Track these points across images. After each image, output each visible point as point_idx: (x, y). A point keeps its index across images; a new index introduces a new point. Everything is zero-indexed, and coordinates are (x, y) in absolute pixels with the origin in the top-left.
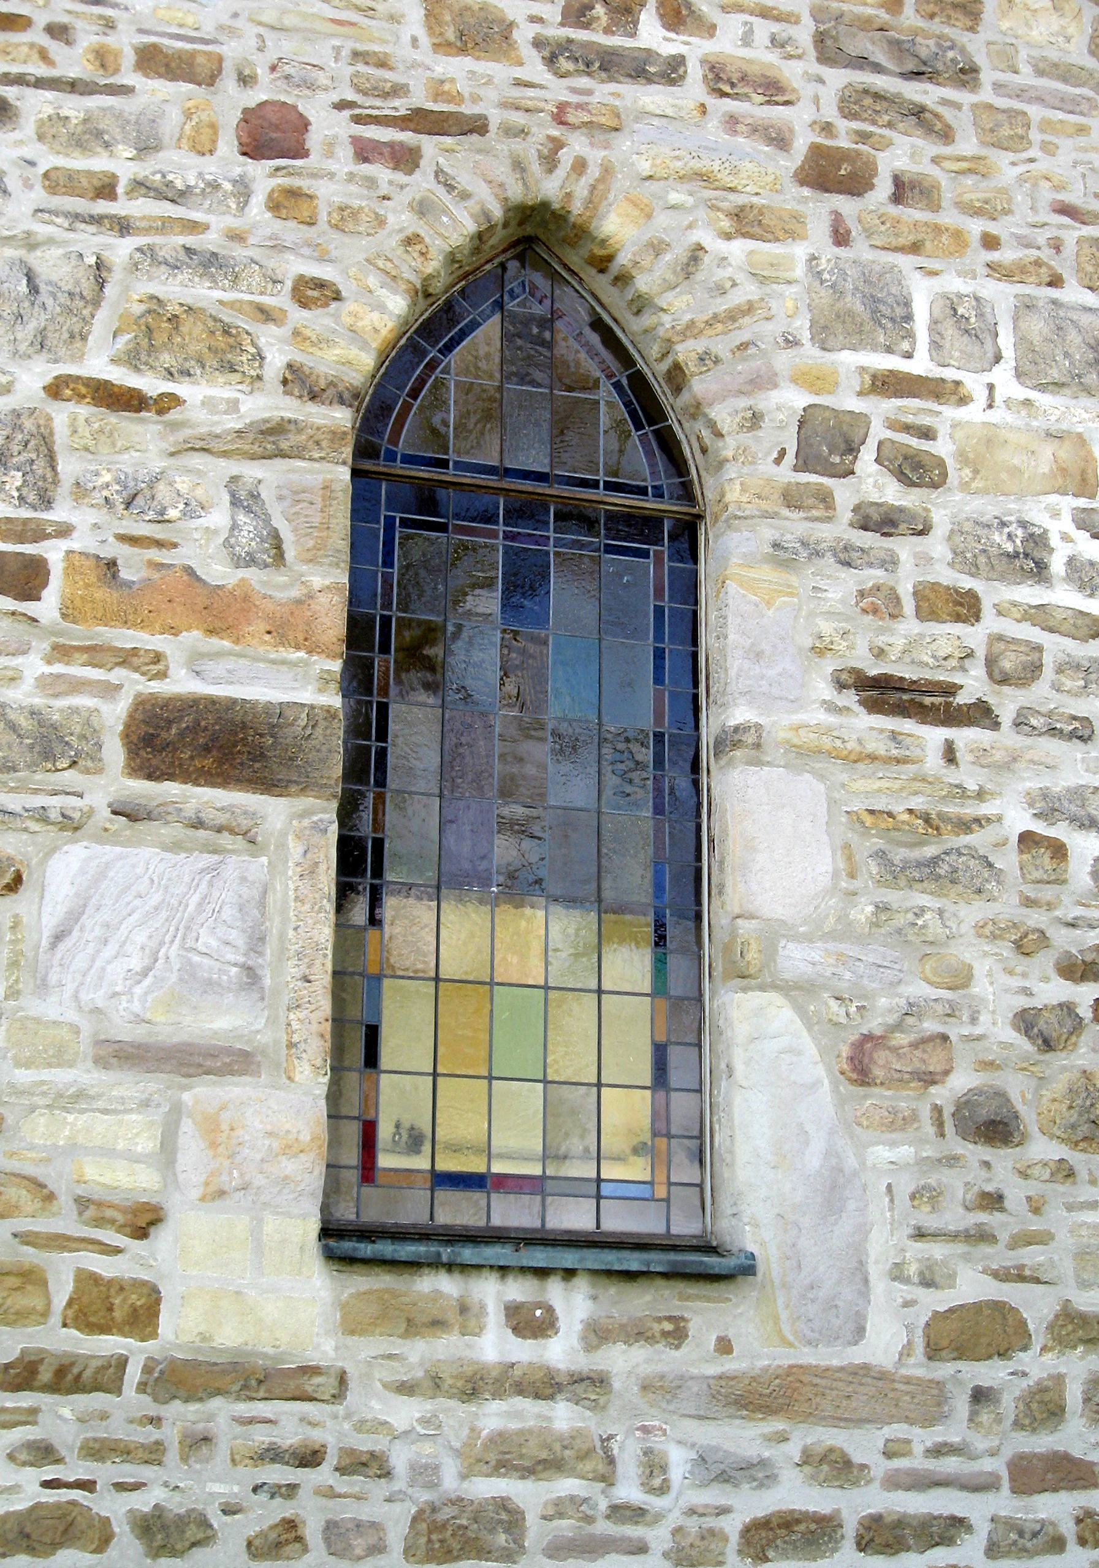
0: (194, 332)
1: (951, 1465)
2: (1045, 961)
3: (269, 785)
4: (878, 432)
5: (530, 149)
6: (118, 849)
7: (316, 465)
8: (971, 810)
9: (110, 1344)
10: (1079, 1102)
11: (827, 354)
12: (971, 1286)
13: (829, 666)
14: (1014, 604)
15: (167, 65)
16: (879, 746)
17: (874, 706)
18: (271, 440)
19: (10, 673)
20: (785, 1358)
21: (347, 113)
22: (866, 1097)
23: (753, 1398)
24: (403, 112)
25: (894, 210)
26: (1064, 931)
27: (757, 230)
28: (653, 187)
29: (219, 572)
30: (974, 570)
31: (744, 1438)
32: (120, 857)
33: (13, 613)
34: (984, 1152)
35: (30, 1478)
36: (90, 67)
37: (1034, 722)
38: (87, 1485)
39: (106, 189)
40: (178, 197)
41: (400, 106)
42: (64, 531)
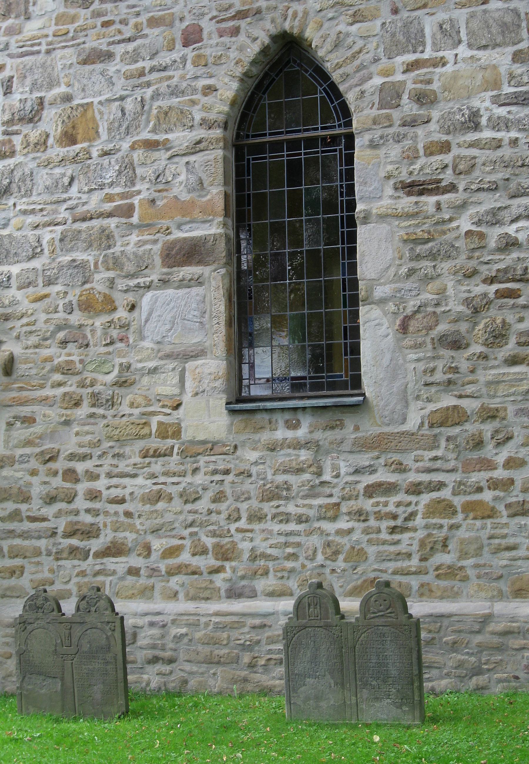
1: (438, 464)
2: (477, 279)
3: (205, 263)
4: (410, 86)
5: (277, 15)
6: (161, 291)
7: (212, 151)
9: (170, 442)
10: (488, 330)
11: (391, 60)
13: (392, 182)
14: (465, 141)
15: (157, 22)
18: (197, 147)
19: (127, 242)
21: (214, 21)
22: (406, 338)
24: (233, 14)
27: (361, 18)
29: (185, 196)
32: (162, 293)
34: (452, 353)
36: (133, 31)
37: (472, 187)
40: (165, 69)
41: (232, 12)
42: (139, 192)
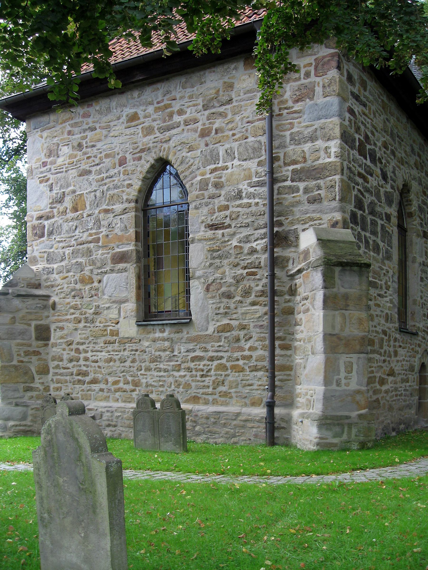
1: (221, 348)
2: (239, 267)
5: (157, 150)
9: (115, 338)
13: (204, 224)
18: (125, 211)
25: (216, 136)
29: (120, 233)
31: (191, 346)
41: (138, 150)
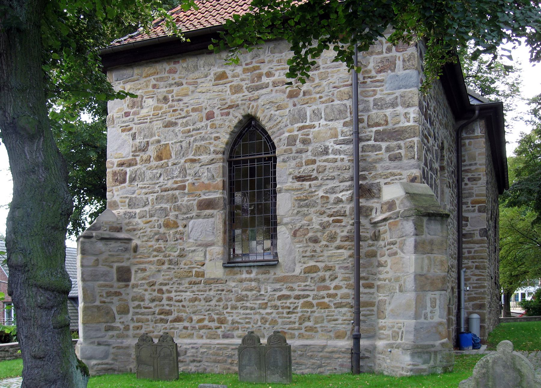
0: (202, 149)
1: (307, 288)
2: (325, 215)
4: (300, 136)
5: (245, 107)
8: (313, 194)
9: (200, 279)
12: (312, 263)
13: (291, 176)
16: (300, 187)
17: (298, 181)
20: (283, 275)
23: (278, 280)
25: (303, 98)
26: (329, 210)
28: (264, 106)
29: (206, 182)
30: (315, 156)
31: (278, 286)
33: (168, 191)
35: (192, 294)
38: (198, 295)
39: (189, 131)
40: (199, 130)
41: (227, 106)
42: (188, 180)
